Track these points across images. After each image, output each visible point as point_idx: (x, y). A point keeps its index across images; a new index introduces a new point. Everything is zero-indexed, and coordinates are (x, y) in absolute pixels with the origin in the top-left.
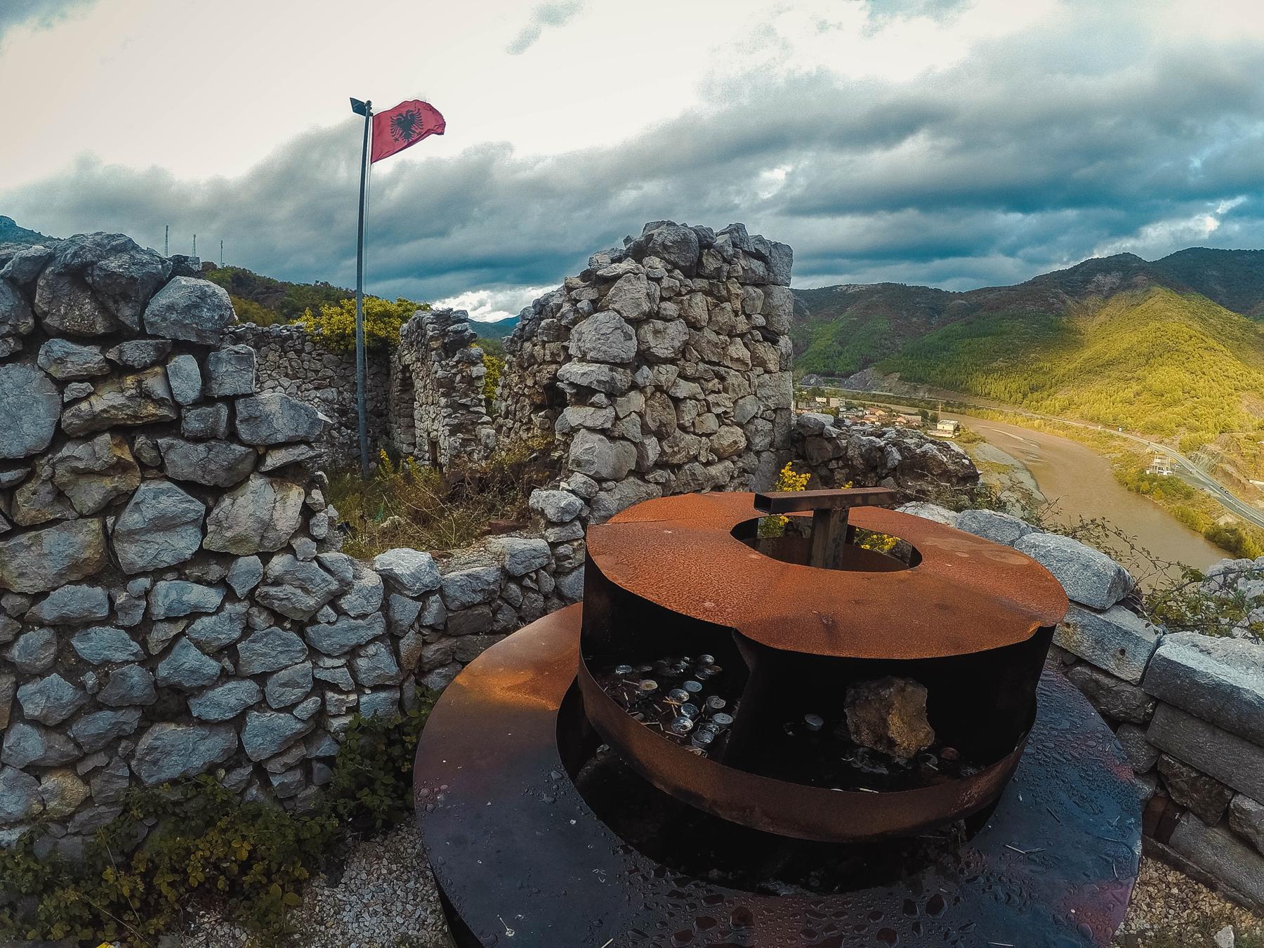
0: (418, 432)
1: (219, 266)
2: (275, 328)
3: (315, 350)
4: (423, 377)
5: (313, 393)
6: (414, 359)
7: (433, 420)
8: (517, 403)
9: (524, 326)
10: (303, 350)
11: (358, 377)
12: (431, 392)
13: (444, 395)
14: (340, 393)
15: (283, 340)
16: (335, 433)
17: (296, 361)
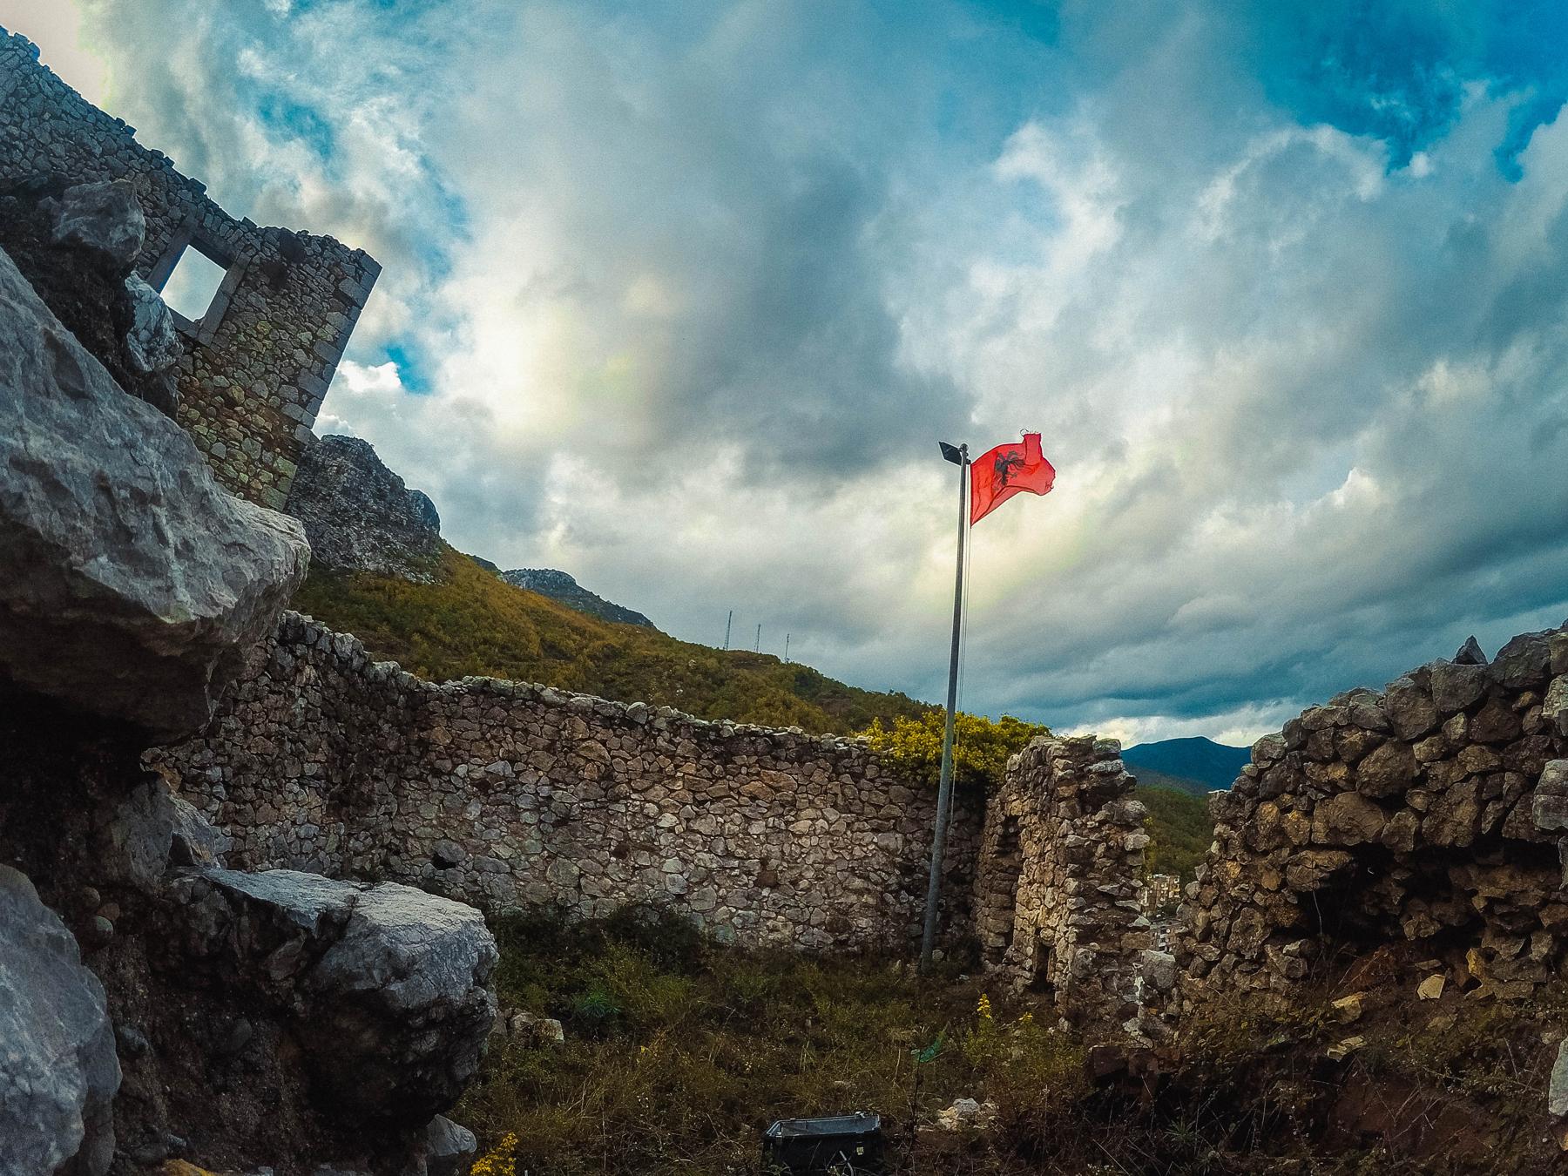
0: (1018, 923)
1: (783, 661)
2: (829, 738)
3: (880, 776)
4: (1039, 840)
5: (868, 837)
6: (1027, 809)
7: (1050, 911)
8: (1233, 918)
9: (1262, 772)
10: (863, 775)
11: (938, 823)
12: (1051, 866)
13: (1074, 875)
14: (907, 842)
15: (837, 757)
16: (890, 898)
17: (851, 788)
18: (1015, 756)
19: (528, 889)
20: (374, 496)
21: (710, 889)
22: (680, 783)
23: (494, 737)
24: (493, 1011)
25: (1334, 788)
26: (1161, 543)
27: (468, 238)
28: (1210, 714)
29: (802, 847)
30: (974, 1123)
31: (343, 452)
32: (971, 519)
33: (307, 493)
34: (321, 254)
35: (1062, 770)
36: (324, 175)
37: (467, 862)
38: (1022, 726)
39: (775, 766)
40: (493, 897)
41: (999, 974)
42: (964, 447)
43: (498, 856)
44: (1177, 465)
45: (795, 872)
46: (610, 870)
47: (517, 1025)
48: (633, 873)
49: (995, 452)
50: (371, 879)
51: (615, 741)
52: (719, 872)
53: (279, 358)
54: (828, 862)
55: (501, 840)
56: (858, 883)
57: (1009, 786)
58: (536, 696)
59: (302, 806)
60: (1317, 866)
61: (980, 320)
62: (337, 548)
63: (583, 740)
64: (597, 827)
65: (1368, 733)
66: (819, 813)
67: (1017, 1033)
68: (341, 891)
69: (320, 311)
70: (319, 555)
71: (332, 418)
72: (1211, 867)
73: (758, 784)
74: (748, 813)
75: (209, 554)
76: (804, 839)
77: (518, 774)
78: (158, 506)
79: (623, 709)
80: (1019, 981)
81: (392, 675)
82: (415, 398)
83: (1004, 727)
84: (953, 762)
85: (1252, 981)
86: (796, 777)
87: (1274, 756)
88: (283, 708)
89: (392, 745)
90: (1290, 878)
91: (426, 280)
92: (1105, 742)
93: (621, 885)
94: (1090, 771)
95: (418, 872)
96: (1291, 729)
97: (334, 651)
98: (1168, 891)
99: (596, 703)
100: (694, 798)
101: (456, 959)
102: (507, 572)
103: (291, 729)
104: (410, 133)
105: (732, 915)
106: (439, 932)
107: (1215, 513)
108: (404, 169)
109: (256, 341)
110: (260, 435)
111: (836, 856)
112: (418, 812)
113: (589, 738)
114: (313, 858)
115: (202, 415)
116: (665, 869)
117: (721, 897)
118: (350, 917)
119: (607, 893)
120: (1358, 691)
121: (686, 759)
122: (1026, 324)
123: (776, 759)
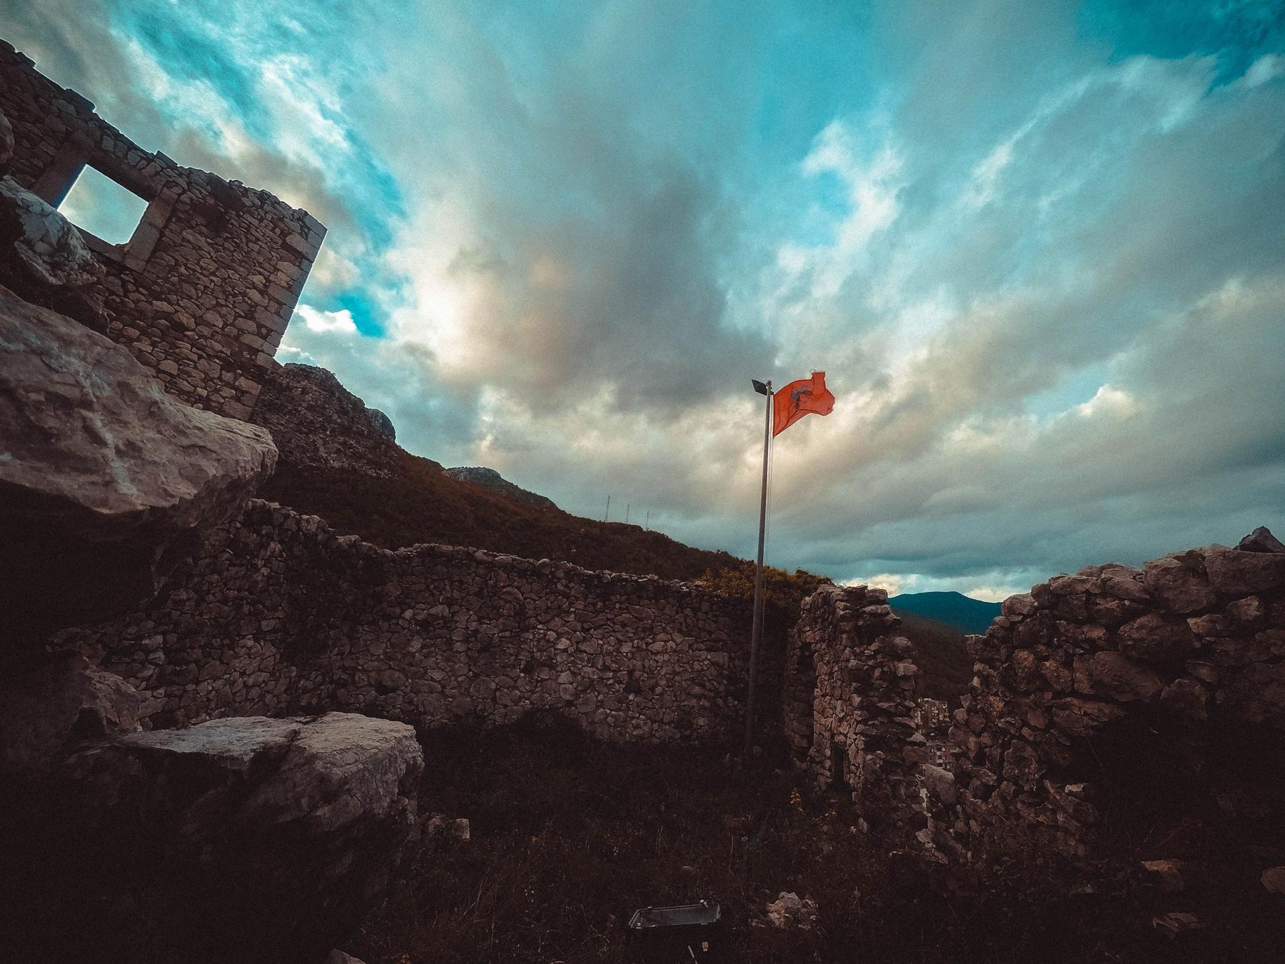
0: (817, 728)
2: (678, 583)
4: (828, 662)
5: (704, 654)
6: (818, 638)
7: (841, 720)
9: (1013, 624)
10: (700, 609)
12: (839, 683)
13: (857, 691)
14: (731, 659)
15: (681, 596)
16: (720, 701)
18: (807, 598)
19: (454, 704)
20: (337, 412)
21: (591, 695)
22: (573, 616)
23: (435, 587)
24: (411, 817)
25: (1094, 646)
26: (917, 446)
27: (402, 214)
28: (962, 575)
29: (657, 662)
30: (799, 922)
31: (307, 377)
32: (773, 432)
33: (272, 407)
34: (261, 207)
35: (843, 611)
36: (247, 126)
37: (406, 687)
38: (811, 576)
39: (639, 603)
40: (425, 713)
41: (806, 771)
42: (769, 383)
43: (432, 679)
44: (931, 390)
45: (653, 681)
46: (519, 683)
47: (431, 828)
48: (536, 685)
49: (792, 386)
50: (316, 712)
51: (528, 587)
52: (598, 682)
53: (230, 294)
54: (675, 673)
55: (437, 667)
56: (697, 690)
57: (803, 620)
58: (470, 556)
59: (255, 658)
60: (1086, 713)
61: (783, 290)
62: (304, 451)
63: (504, 587)
64: (511, 651)
65: (1127, 603)
66: (669, 637)
67: (825, 828)
68: (284, 727)
69: (270, 260)
70: (286, 456)
71: (294, 350)
72: (975, 698)
73: (628, 615)
74: (620, 637)
75: (164, 453)
76: (659, 656)
77: (454, 614)
78: (89, 410)
79: (533, 564)
80: (822, 779)
81: (353, 545)
82: (370, 340)
83: (798, 577)
84: (762, 601)
85: (1037, 815)
86: (653, 610)
87: (1025, 612)
88: (244, 577)
89: (349, 599)
90: (1057, 719)
91: (370, 246)
92: (874, 591)
93: (526, 695)
94: (864, 612)
95: (362, 700)
96: (1039, 592)
97: (299, 529)
98: (938, 714)
99: (515, 560)
100: (582, 626)
101: (385, 774)
102: (450, 469)
103: (251, 593)
104: (332, 103)
105: (607, 715)
106: (374, 750)
107: (963, 426)
108: (332, 140)
109: (200, 276)
110: (218, 358)
111: (682, 669)
112: (368, 650)
113: (509, 586)
114: (259, 701)
115: (142, 334)
116: (560, 680)
117: (599, 701)
118: (287, 752)
119: (516, 704)
120: (1111, 566)
121: (577, 599)
122: (817, 292)
123: (640, 597)
